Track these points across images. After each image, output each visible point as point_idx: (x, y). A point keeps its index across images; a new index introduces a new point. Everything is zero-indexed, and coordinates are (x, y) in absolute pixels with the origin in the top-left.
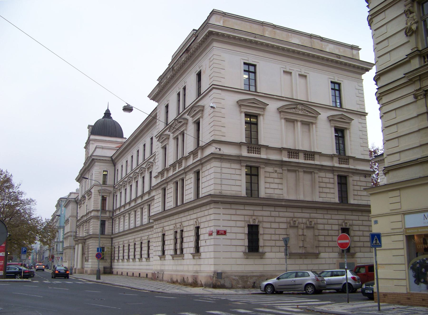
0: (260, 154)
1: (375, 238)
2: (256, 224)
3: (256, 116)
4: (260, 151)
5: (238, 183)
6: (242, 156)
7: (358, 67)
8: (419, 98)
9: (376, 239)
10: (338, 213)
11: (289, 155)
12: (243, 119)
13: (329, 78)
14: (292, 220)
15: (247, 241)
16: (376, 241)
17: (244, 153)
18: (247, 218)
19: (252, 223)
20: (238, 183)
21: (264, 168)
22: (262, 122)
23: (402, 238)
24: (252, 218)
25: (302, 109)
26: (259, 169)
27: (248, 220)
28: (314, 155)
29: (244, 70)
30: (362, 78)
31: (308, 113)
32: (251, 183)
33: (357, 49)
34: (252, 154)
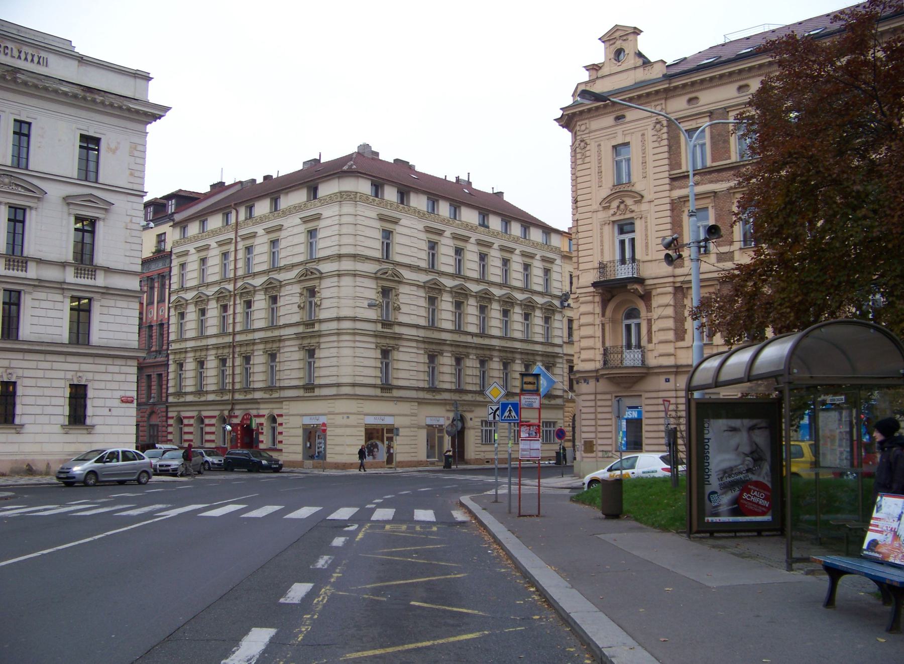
0: (26, 271)
1: (508, 409)
2: (13, 380)
3: (93, 222)
4: (95, 275)
5: (104, 326)
6: (64, 283)
7: (146, 114)
9: (510, 410)
10: (24, 357)
11: (77, 273)
12: (72, 225)
13: (11, 113)
14: (6, 372)
15: (67, 409)
16: (510, 413)
17: (70, 276)
18: (69, 375)
19: (76, 383)
20: (104, 326)
21: (30, 293)
22: (32, 220)
23: (363, 429)
24: (6, 372)
25: (10, 182)
26: (92, 300)
27: (71, 378)
28: (95, 271)
29: (14, 132)
30: (146, 130)
31: (23, 190)
32: (78, 322)
33: (147, 78)
34: (20, 272)
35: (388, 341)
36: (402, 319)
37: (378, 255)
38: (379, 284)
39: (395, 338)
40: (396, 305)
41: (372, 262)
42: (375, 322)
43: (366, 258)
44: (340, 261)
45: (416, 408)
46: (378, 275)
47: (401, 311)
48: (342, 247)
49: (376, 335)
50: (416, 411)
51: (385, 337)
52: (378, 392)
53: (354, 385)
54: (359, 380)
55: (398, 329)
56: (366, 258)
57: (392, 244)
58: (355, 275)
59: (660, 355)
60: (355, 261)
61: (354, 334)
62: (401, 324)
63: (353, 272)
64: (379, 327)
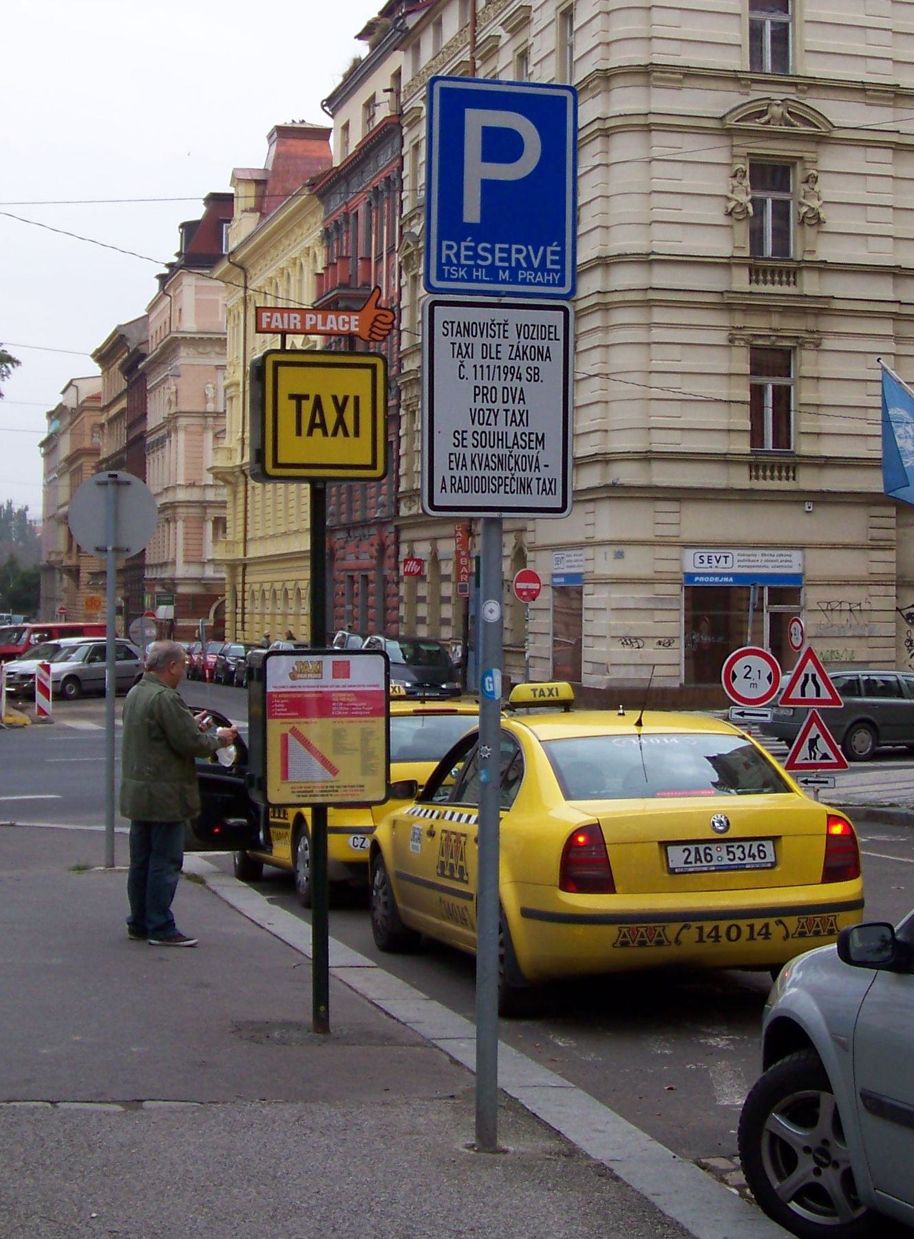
8: (737, 343)
35: (776, 321)
36: (829, 251)
37: (739, 61)
38: (737, 151)
39: (802, 312)
40: (805, 209)
41: (713, 84)
42: (727, 264)
43: (685, 75)
44: (608, 90)
45: (892, 522)
46: (731, 122)
47: (825, 228)
48: (614, 47)
49: (727, 303)
50: (892, 534)
51: (766, 310)
52: (740, 479)
53: (647, 457)
54: (663, 442)
55: (811, 284)
56: (685, 75)
57: (794, 25)
58: (648, 128)
59: (289, 275)
60: (648, 86)
61: (649, 304)
62: (824, 268)
63: (641, 120)
64: (740, 281)
